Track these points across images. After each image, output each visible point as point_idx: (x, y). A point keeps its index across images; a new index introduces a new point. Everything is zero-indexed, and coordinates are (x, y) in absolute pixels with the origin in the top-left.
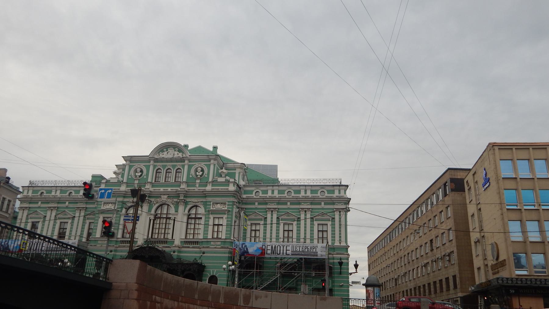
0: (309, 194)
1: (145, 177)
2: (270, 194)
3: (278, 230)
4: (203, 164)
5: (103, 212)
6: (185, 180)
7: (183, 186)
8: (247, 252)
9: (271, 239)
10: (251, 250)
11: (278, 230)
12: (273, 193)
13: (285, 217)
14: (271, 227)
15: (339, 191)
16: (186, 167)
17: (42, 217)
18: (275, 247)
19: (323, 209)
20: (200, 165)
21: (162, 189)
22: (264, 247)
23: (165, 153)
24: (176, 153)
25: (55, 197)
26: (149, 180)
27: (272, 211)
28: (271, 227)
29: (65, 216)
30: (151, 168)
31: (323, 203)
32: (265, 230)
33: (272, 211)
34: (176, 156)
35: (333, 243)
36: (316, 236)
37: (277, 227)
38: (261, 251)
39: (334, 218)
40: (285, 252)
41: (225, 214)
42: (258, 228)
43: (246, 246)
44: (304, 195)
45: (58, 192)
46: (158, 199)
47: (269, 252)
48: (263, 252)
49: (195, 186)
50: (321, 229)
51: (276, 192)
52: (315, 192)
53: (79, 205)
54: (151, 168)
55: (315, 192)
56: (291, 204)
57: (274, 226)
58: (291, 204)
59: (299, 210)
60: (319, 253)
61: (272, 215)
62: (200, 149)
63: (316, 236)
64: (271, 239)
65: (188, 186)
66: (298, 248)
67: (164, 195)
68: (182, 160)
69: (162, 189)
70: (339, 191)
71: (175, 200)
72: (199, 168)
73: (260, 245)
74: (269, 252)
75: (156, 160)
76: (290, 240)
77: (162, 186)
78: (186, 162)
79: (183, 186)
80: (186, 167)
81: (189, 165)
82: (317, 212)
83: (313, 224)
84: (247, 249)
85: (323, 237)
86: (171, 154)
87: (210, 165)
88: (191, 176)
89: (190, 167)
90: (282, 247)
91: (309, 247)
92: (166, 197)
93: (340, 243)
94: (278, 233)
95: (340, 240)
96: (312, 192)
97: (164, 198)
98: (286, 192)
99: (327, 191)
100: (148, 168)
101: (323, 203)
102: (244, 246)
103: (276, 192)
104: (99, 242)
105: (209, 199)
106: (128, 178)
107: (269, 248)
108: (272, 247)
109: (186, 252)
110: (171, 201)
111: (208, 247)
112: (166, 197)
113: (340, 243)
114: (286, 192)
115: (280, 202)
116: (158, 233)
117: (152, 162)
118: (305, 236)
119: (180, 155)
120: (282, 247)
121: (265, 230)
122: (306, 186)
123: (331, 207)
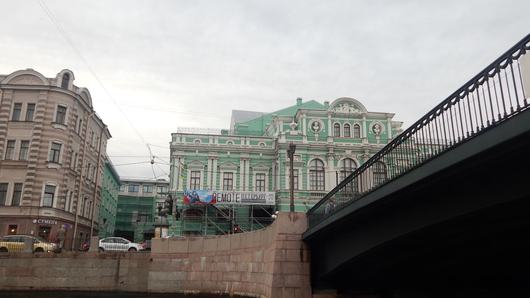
0: (184, 141)
1: (324, 131)
2: (243, 143)
3: (218, 178)
4: (319, 119)
6: (365, 136)
7: (366, 142)
8: (198, 200)
9: (244, 188)
10: (202, 198)
11: (218, 178)
12: (245, 143)
13: (257, 167)
14: (212, 175)
16: (364, 124)
17: (204, 166)
18: (226, 195)
20: (316, 120)
21: (344, 144)
22: (215, 195)
23: (341, 108)
24: (352, 109)
25: (213, 146)
26: (330, 134)
27: (213, 160)
28: (212, 175)
29: (227, 166)
30: (330, 122)
31: (197, 151)
32: (238, 179)
33: (245, 161)
34: (352, 112)
36: (254, 185)
38: (211, 199)
39: (206, 166)
40: (235, 199)
41: (301, 166)
42: (262, 178)
43: (196, 194)
44: (212, 143)
45: (184, 140)
46: (343, 154)
47: (220, 199)
48: (214, 200)
49: (376, 142)
50: (193, 176)
51: (248, 143)
52: (191, 140)
53: (242, 156)
54: (330, 122)
55: (191, 140)
56: (200, 152)
57: (215, 174)
58: (200, 152)
59: (239, 159)
60: (267, 199)
61: (245, 164)
62: (313, 103)
63: (254, 185)
64: (244, 188)
65: (334, 140)
66: (248, 196)
67: (348, 149)
68: (360, 117)
69: (344, 144)
71: (361, 155)
72: (378, 125)
73: (210, 193)
74: (220, 199)
75: (334, 115)
76: (262, 189)
77: (353, 141)
78: (364, 118)
79: (366, 142)
80: (364, 124)
81: (367, 122)
82: (255, 162)
84: (198, 197)
85: (260, 186)
86: (345, 110)
87: (387, 123)
88: (370, 133)
89: (368, 124)
90: (232, 195)
91: (258, 195)
92: (350, 151)
94: (218, 181)
96: (187, 140)
97: (349, 152)
98: (195, 140)
99: (266, 142)
100: (326, 122)
101: (197, 151)
102: (194, 193)
103: (248, 143)
106: (307, 132)
107: (220, 196)
108: (223, 195)
110: (355, 156)
112: (350, 151)
114: (195, 140)
117: (330, 117)
118: (244, 185)
119: (357, 111)
120: (232, 195)
121: (238, 179)
122: (214, 135)
123: (206, 155)
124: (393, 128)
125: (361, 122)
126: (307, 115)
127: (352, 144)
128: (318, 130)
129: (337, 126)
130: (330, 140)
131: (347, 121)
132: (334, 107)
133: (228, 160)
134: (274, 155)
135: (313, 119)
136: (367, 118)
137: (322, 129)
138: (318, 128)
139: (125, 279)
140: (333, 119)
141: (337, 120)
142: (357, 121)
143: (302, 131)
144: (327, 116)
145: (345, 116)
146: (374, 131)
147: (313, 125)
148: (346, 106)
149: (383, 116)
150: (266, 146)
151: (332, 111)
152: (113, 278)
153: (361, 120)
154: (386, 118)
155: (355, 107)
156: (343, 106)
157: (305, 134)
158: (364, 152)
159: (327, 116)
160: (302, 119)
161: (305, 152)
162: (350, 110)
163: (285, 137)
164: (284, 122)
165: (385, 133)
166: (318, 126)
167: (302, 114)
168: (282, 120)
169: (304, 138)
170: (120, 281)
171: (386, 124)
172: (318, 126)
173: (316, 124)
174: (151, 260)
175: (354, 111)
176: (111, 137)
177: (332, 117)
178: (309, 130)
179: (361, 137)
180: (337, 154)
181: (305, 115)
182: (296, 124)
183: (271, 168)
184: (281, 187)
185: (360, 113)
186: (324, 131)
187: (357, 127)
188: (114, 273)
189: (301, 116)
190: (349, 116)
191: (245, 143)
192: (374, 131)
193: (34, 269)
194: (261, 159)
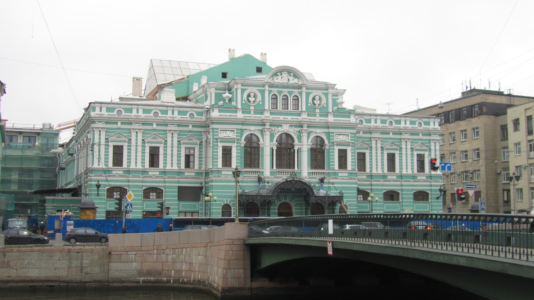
1: (261, 103)
4: (319, 93)
5: (223, 140)
6: (304, 109)
12: (173, 114)
15: (138, 110)
16: (304, 95)
19: (119, 129)
24: (291, 78)
26: (267, 107)
35: (401, 172)
37: (105, 148)
39: (130, 140)
41: (234, 142)
46: (279, 128)
49: (315, 115)
54: (267, 93)
56: (157, 125)
65: (308, 115)
68: (300, 87)
69: (281, 117)
70: (138, 110)
75: (271, 86)
77: (291, 114)
78: (304, 89)
79: (304, 116)
80: (304, 95)
81: (306, 93)
83: (180, 148)
88: (309, 105)
89: (308, 95)
93: (136, 166)
95: (172, 164)
96: (108, 110)
99: (196, 112)
100: (263, 92)
104: (223, 173)
105: (331, 130)
109: (216, 181)
111: (336, 178)
113: (136, 166)
115: (384, 132)
116: (78, 159)
117: (267, 87)
119: (296, 81)
124: (334, 96)
125: (301, 93)
126: (242, 85)
127: (289, 118)
128: (254, 102)
129: (275, 98)
130: (267, 114)
131: (285, 91)
132: (272, 76)
133: (154, 132)
134: (205, 127)
135: (249, 90)
136: (306, 89)
137: (258, 100)
138: (253, 99)
139: (88, 270)
140: (270, 89)
141: (275, 91)
142: (296, 92)
143: (237, 103)
144: (263, 86)
145: (283, 86)
146: (313, 103)
147: (249, 96)
148: (285, 75)
149: (324, 86)
150: (195, 116)
151: (269, 81)
152: (78, 268)
153: (300, 91)
154: (327, 89)
155: (295, 76)
156: (281, 74)
157: (239, 106)
158: (302, 127)
159: (264, 86)
160: (236, 89)
161: (240, 127)
162: (289, 80)
163: (218, 110)
164: (216, 89)
165: (325, 105)
166: (254, 97)
167: (237, 84)
168: (213, 87)
169: (238, 111)
170: (84, 271)
171: (326, 95)
172: (254, 97)
173: (252, 95)
174: (110, 253)
175: (293, 81)
176: (5, 93)
177: (269, 87)
178: (243, 102)
179: (300, 110)
180: (273, 128)
181: (240, 86)
182: (230, 96)
183: (201, 142)
184: (213, 165)
185: (300, 83)
186: (261, 103)
187: (296, 99)
188: (79, 265)
189: (236, 86)
190: (287, 87)
191: (173, 114)
192: (313, 103)
193: (9, 262)
194: (190, 131)
